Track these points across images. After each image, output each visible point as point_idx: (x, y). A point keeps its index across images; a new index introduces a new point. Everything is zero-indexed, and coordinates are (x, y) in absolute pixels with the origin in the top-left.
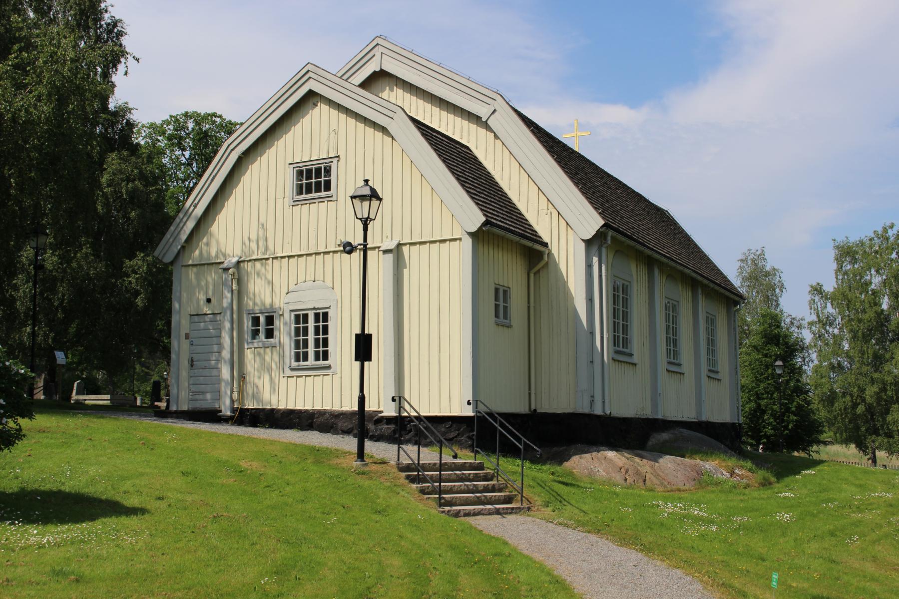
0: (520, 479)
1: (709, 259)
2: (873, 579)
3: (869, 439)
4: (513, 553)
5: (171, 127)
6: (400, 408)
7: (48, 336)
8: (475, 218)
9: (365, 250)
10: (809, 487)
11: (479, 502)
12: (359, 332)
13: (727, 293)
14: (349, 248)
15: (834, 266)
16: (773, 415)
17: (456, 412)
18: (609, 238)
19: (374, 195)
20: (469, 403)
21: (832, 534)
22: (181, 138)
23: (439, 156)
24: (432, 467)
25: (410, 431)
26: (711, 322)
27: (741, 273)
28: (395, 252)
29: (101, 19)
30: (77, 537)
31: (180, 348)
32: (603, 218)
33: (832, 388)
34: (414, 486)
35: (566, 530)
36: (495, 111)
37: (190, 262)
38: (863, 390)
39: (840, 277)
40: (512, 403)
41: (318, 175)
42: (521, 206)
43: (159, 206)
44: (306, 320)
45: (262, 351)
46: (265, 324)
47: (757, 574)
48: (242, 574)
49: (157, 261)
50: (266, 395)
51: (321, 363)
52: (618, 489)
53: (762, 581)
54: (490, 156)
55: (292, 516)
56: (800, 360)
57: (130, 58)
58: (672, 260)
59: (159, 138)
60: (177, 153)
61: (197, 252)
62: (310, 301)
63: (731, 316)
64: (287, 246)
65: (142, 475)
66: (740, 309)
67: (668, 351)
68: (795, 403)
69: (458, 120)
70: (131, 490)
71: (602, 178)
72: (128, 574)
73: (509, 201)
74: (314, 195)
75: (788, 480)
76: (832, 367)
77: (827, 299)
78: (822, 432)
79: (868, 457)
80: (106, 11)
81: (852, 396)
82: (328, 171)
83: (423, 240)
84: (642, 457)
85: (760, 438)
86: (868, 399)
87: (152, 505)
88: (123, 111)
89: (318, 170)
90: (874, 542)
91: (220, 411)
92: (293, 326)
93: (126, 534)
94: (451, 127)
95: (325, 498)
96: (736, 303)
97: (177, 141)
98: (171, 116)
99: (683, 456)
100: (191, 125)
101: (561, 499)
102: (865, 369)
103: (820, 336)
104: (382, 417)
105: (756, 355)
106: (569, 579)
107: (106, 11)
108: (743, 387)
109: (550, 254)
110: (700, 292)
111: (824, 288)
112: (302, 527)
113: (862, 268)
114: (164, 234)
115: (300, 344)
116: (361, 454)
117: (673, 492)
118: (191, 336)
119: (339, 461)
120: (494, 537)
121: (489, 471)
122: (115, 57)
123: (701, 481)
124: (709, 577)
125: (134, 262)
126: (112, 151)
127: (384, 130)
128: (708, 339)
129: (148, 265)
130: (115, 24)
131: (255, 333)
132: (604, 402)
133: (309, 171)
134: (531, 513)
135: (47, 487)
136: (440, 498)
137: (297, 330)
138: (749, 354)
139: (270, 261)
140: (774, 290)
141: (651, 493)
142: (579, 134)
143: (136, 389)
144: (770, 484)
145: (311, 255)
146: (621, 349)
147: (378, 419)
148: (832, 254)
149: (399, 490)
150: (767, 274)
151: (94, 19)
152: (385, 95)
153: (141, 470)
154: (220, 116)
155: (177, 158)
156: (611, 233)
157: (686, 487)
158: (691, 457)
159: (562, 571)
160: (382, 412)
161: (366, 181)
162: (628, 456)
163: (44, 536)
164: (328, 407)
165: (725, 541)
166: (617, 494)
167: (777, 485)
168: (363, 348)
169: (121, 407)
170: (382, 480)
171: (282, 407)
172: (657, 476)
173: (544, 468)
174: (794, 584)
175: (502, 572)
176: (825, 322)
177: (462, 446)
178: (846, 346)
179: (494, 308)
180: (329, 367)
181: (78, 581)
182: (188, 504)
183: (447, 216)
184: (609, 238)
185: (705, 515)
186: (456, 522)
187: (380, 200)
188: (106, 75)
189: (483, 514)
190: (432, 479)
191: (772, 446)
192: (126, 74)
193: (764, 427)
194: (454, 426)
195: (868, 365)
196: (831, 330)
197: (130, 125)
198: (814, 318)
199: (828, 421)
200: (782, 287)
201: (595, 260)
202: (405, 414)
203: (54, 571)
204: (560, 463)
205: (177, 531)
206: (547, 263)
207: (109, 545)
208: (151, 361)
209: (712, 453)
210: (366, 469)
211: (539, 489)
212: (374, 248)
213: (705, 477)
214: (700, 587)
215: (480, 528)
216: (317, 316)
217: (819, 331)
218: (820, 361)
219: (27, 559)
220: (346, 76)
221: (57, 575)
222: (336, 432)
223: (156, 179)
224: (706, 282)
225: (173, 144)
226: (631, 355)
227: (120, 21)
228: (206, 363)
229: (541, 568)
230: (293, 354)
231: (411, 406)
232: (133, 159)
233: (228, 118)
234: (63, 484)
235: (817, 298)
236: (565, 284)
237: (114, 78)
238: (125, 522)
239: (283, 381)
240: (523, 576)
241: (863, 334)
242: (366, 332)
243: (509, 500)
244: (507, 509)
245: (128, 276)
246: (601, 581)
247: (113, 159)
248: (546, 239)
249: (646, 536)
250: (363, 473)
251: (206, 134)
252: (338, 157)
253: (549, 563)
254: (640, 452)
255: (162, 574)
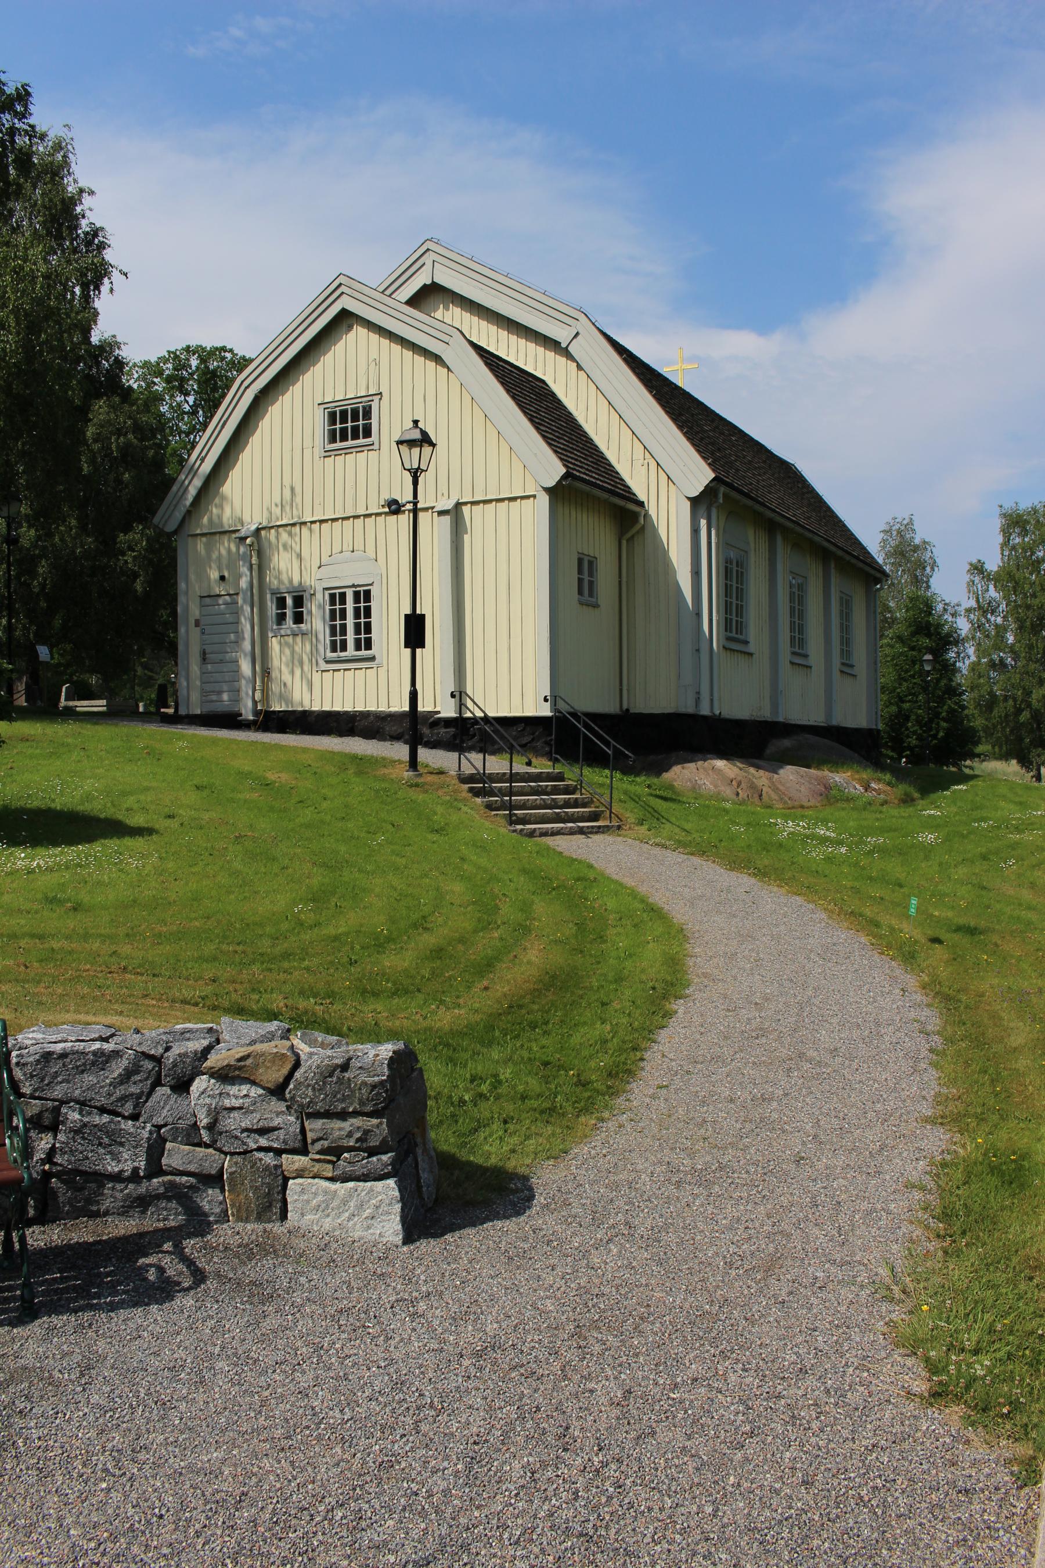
0: (608, 792)
1: (844, 525)
2: (1029, 908)
3: (1034, 752)
4: (599, 878)
5: (170, 366)
6: (461, 705)
7: (28, 629)
8: (554, 470)
9: (415, 511)
10: (959, 804)
11: (558, 819)
12: (408, 612)
13: (867, 569)
14: (394, 507)
15: (1000, 539)
16: (919, 722)
17: (530, 712)
18: (721, 495)
19: (425, 440)
20: (546, 700)
21: (984, 857)
22: (182, 380)
23: (508, 391)
24: (500, 778)
25: (474, 735)
26: (846, 605)
27: (884, 547)
28: (453, 513)
29: (77, 227)
30: (73, 860)
31: (190, 639)
32: (713, 470)
33: (992, 690)
34: (479, 800)
35: (664, 851)
36: (577, 334)
37: (198, 532)
38: (1029, 694)
39: (1006, 553)
40: (597, 700)
41: (355, 418)
42: (611, 456)
43: (158, 464)
44: (343, 601)
45: (290, 639)
46: (293, 605)
47: (892, 902)
48: (271, 902)
49: (160, 532)
50: (296, 696)
51: (363, 653)
52: (728, 805)
53: (898, 909)
54: (572, 393)
55: (330, 835)
56: (953, 655)
57: (116, 275)
58: (799, 524)
59: (155, 380)
60: (178, 399)
61: (205, 520)
62: (348, 575)
63: (871, 597)
64: (318, 509)
65: (147, 789)
66: (881, 588)
67: (793, 639)
68: (946, 707)
69: (531, 346)
70: (135, 806)
71: (713, 421)
72: (134, 901)
73: (596, 448)
74: (350, 443)
75: (933, 796)
76: (992, 665)
77: (989, 580)
78: (977, 743)
79: (1032, 774)
80: (84, 217)
81: (1015, 700)
82: (368, 413)
83: (488, 497)
84: (758, 767)
85: (904, 749)
86: (1035, 704)
87: (161, 824)
88: (108, 347)
89: (355, 413)
90: (1034, 866)
91: (241, 715)
92: (328, 607)
93: (131, 857)
94: (522, 355)
95: (370, 815)
96: (878, 581)
97: (177, 383)
98: (169, 352)
99: (808, 767)
100: (194, 362)
101: (657, 816)
102: (1032, 666)
103: (979, 627)
104: (440, 719)
105: (900, 648)
106: (666, 907)
107: (84, 217)
108: (883, 687)
109: (646, 515)
110: (833, 566)
111: (986, 566)
112: (343, 848)
113: (1034, 541)
114: (163, 499)
115: (337, 631)
116: (413, 763)
117: (794, 809)
118: (202, 623)
119: (386, 771)
120: (576, 860)
121: (570, 782)
122: (96, 275)
123: (830, 796)
124: (835, 905)
125: (130, 536)
126: (98, 396)
127: (437, 359)
128: (842, 624)
129: (148, 540)
130: (96, 232)
131: (281, 618)
132: (712, 700)
133: (344, 413)
134: (622, 832)
135: (35, 804)
136: (511, 815)
137: (333, 612)
138: (892, 647)
139: (298, 527)
140: (924, 568)
141: (768, 810)
142: (684, 367)
143: (137, 696)
144: (913, 800)
145: (348, 518)
146: (733, 635)
147: (434, 721)
148: (997, 523)
149: (460, 805)
150: (916, 548)
151: (69, 227)
152: (439, 314)
153: (145, 784)
154: (231, 351)
155: (179, 405)
156: (722, 489)
157: (810, 804)
158: (818, 768)
159: (658, 899)
160: (439, 712)
161: (416, 422)
162: (741, 766)
163: (33, 860)
164: (372, 708)
165: (856, 864)
166: (726, 811)
167: (921, 802)
168: (415, 631)
169: (120, 712)
170: (440, 793)
171: (316, 708)
172: (776, 790)
173: (638, 779)
174: (936, 913)
175: (586, 899)
176: (986, 609)
177: (538, 753)
178: (1011, 639)
179: (576, 583)
180: (373, 659)
181: (75, 909)
182: (203, 823)
183: (518, 466)
184: (721, 495)
185: (833, 835)
186: (530, 844)
187: (433, 445)
188: (86, 298)
189: (563, 834)
190: (501, 792)
191: (916, 759)
192: (112, 290)
193: (908, 736)
194: (528, 729)
195: (1036, 663)
196: (993, 619)
197: (119, 363)
198: (973, 603)
199: (986, 729)
200: (934, 565)
201: (703, 522)
202: (469, 715)
203: (47, 898)
204: (658, 774)
205: (192, 854)
206: (643, 528)
207: (111, 870)
208: (155, 662)
209: (843, 764)
210: (420, 780)
211: (632, 804)
212: (426, 509)
213: (833, 792)
214: (824, 916)
215: (559, 849)
216: (357, 594)
217: (978, 620)
218: (978, 657)
219: (14, 885)
220: (389, 290)
221: (51, 902)
222: (383, 739)
223: (153, 432)
224: (840, 553)
225: (173, 388)
226: (746, 643)
227: (102, 229)
228: (220, 656)
229: (634, 894)
230: (328, 642)
231: (475, 703)
232: (126, 407)
233: (241, 354)
234: (53, 800)
235: (977, 579)
236: (665, 553)
237: (97, 304)
238: (129, 844)
239: (317, 677)
240: (611, 904)
241: (1032, 624)
242: (418, 612)
243: (595, 817)
244: (592, 827)
245: (123, 554)
246: (706, 909)
247: (100, 409)
248: (642, 496)
249: (762, 858)
250: (417, 785)
251: (214, 373)
252: (381, 393)
253: (643, 889)
254: (756, 761)
255: (175, 902)
